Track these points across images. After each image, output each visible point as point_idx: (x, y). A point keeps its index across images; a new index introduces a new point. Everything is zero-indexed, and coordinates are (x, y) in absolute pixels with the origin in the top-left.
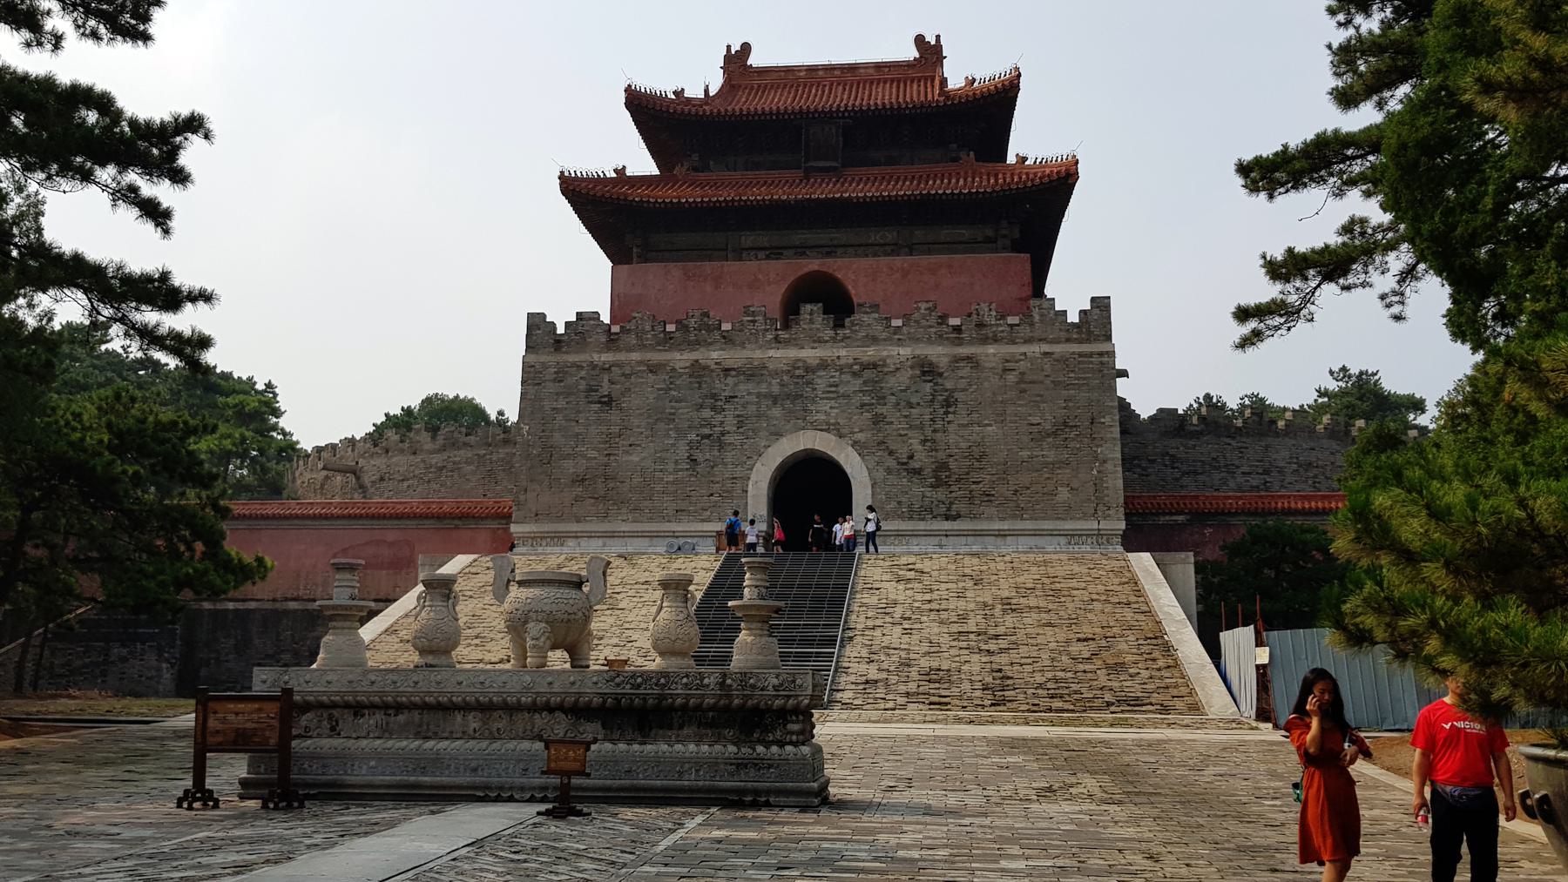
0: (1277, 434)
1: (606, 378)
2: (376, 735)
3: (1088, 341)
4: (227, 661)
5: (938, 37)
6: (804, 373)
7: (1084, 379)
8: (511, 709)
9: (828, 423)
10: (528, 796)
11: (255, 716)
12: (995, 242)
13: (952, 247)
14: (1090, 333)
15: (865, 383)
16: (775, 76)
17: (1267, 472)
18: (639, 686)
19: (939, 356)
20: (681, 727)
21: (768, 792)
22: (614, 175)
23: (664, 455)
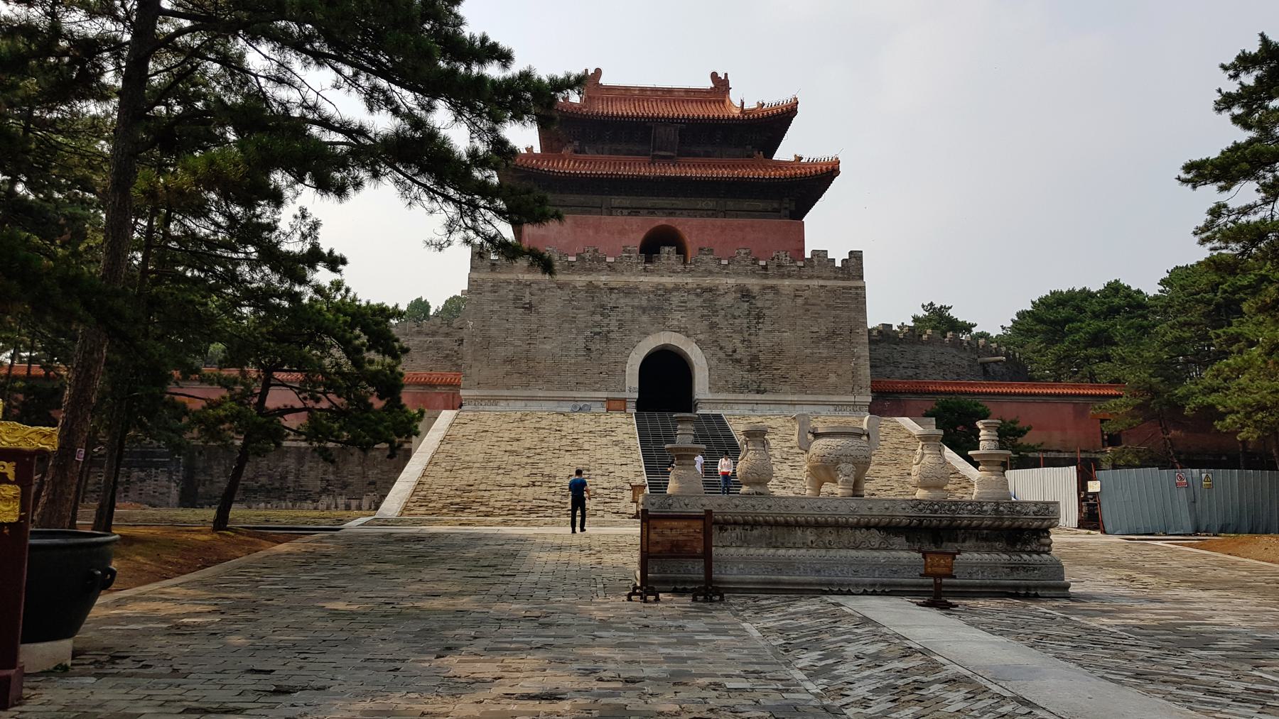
0: (923, 343)
1: (528, 291)
2: (738, 544)
3: (848, 279)
4: (218, 482)
5: (726, 74)
6: (664, 293)
7: (847, 303)
8: (838, 526)
9: (680, 328)
10: (862, 590)
11: (685, 531)
12: (779, 212)
13: (750, 213)
14: (849, 274)
15: (704, 301)
16: (617, 92)
17: (917, 367)
18: (936, 511)
19: (753, 285)
20: (964, 541)
21: (1036, 587)
22: (525, 152)
23: (568, 345)
